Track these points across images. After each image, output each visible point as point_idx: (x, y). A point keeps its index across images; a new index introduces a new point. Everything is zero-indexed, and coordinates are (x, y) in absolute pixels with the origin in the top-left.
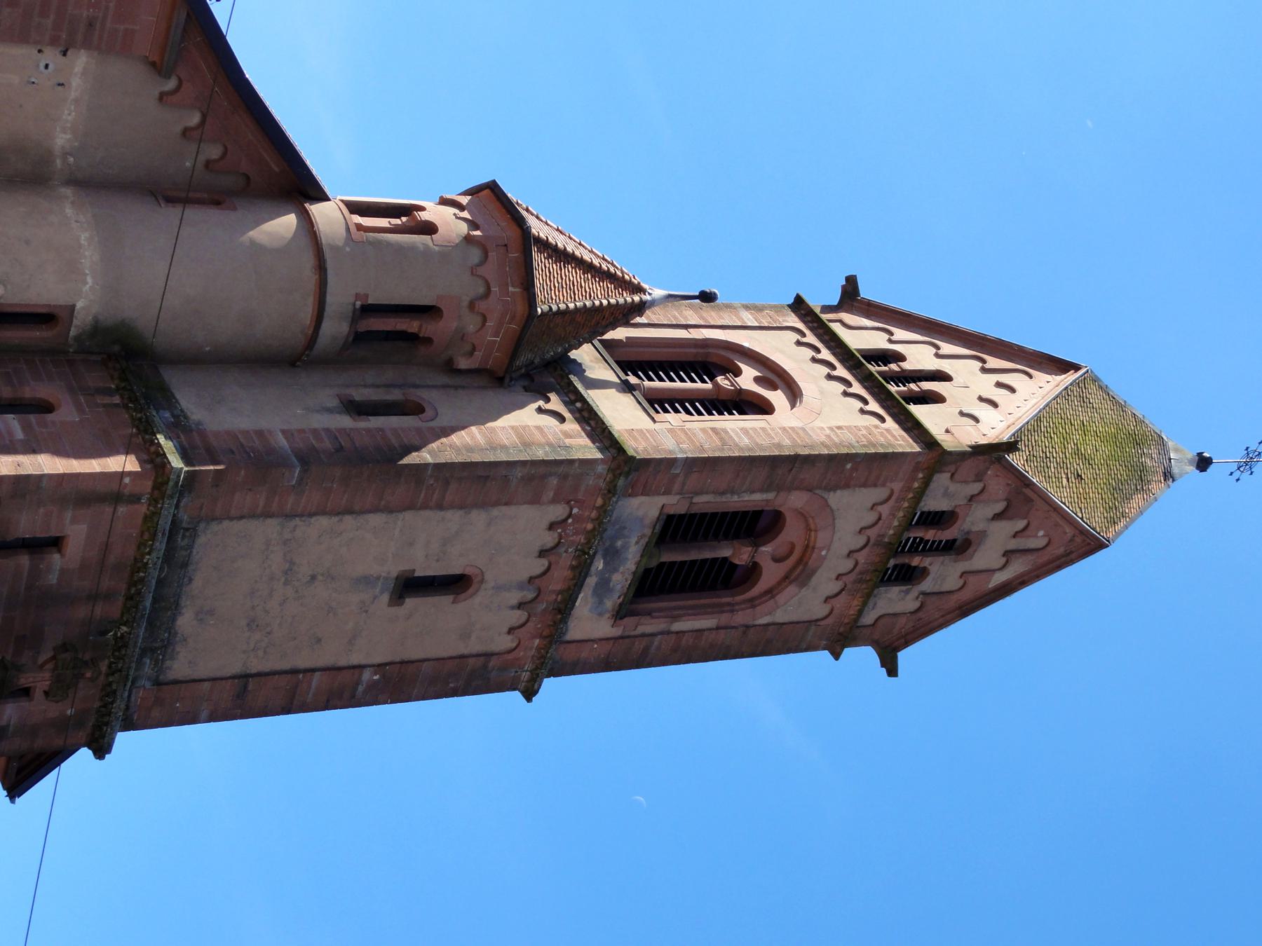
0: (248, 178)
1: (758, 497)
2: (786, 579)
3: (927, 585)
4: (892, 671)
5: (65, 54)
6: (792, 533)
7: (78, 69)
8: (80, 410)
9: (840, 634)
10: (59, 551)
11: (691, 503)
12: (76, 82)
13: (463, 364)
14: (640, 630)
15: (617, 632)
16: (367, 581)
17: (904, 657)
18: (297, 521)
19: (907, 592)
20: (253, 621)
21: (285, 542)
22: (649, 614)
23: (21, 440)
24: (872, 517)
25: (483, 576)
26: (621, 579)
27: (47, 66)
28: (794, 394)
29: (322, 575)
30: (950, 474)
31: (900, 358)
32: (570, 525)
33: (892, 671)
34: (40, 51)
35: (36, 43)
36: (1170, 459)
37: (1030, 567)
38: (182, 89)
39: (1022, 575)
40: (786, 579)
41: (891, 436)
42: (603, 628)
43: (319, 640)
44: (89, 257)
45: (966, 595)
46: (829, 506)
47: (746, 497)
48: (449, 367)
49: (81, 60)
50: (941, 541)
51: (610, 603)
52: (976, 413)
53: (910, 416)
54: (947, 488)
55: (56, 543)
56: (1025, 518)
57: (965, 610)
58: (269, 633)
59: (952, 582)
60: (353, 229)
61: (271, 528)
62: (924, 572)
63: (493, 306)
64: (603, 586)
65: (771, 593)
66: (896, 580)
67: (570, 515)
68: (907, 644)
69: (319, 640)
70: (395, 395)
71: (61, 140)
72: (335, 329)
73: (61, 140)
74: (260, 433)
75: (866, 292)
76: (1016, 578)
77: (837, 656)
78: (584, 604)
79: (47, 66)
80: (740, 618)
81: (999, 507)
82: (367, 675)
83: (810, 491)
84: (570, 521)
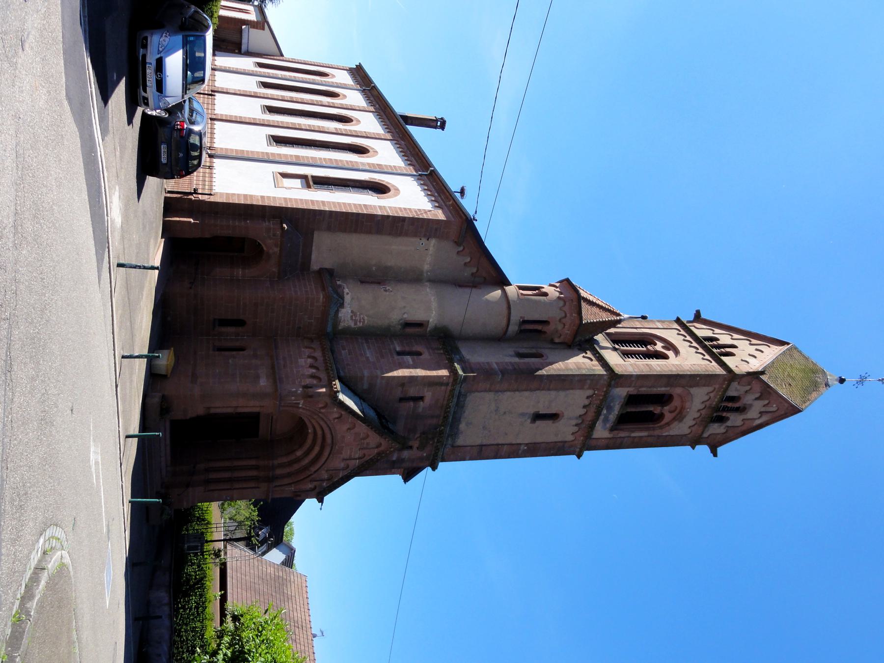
2: (674, 419)
3: (729, 423)
4: (715, 455)
5: (428, 240)
6: (676, 403)
7: (432, 245)
10: (423, 401)
12: (431, 248)
13: (557, 340)
16: (523, 415)
21: (496, 400)
28: (677, 352)
33: (715, 455)
34: (420, 239)
35: (419, 237)
39: (768, 421)
45: (744, 428)
48: (552, 342)
49: (433, 241)
51: (608, 425)
52: (747, 360)
59: (739, 422)
62: (727, 419)
63: (567, 321)
64: (606, 420)
65: (668, 424)
71: (426, 267)
72: (513, 328)
73: (426, 267)
74: (488, 363)
75: (703, 316)
76: (764, 422)
77: (693, 448)
82: (522, 447)
83: (683, 387)
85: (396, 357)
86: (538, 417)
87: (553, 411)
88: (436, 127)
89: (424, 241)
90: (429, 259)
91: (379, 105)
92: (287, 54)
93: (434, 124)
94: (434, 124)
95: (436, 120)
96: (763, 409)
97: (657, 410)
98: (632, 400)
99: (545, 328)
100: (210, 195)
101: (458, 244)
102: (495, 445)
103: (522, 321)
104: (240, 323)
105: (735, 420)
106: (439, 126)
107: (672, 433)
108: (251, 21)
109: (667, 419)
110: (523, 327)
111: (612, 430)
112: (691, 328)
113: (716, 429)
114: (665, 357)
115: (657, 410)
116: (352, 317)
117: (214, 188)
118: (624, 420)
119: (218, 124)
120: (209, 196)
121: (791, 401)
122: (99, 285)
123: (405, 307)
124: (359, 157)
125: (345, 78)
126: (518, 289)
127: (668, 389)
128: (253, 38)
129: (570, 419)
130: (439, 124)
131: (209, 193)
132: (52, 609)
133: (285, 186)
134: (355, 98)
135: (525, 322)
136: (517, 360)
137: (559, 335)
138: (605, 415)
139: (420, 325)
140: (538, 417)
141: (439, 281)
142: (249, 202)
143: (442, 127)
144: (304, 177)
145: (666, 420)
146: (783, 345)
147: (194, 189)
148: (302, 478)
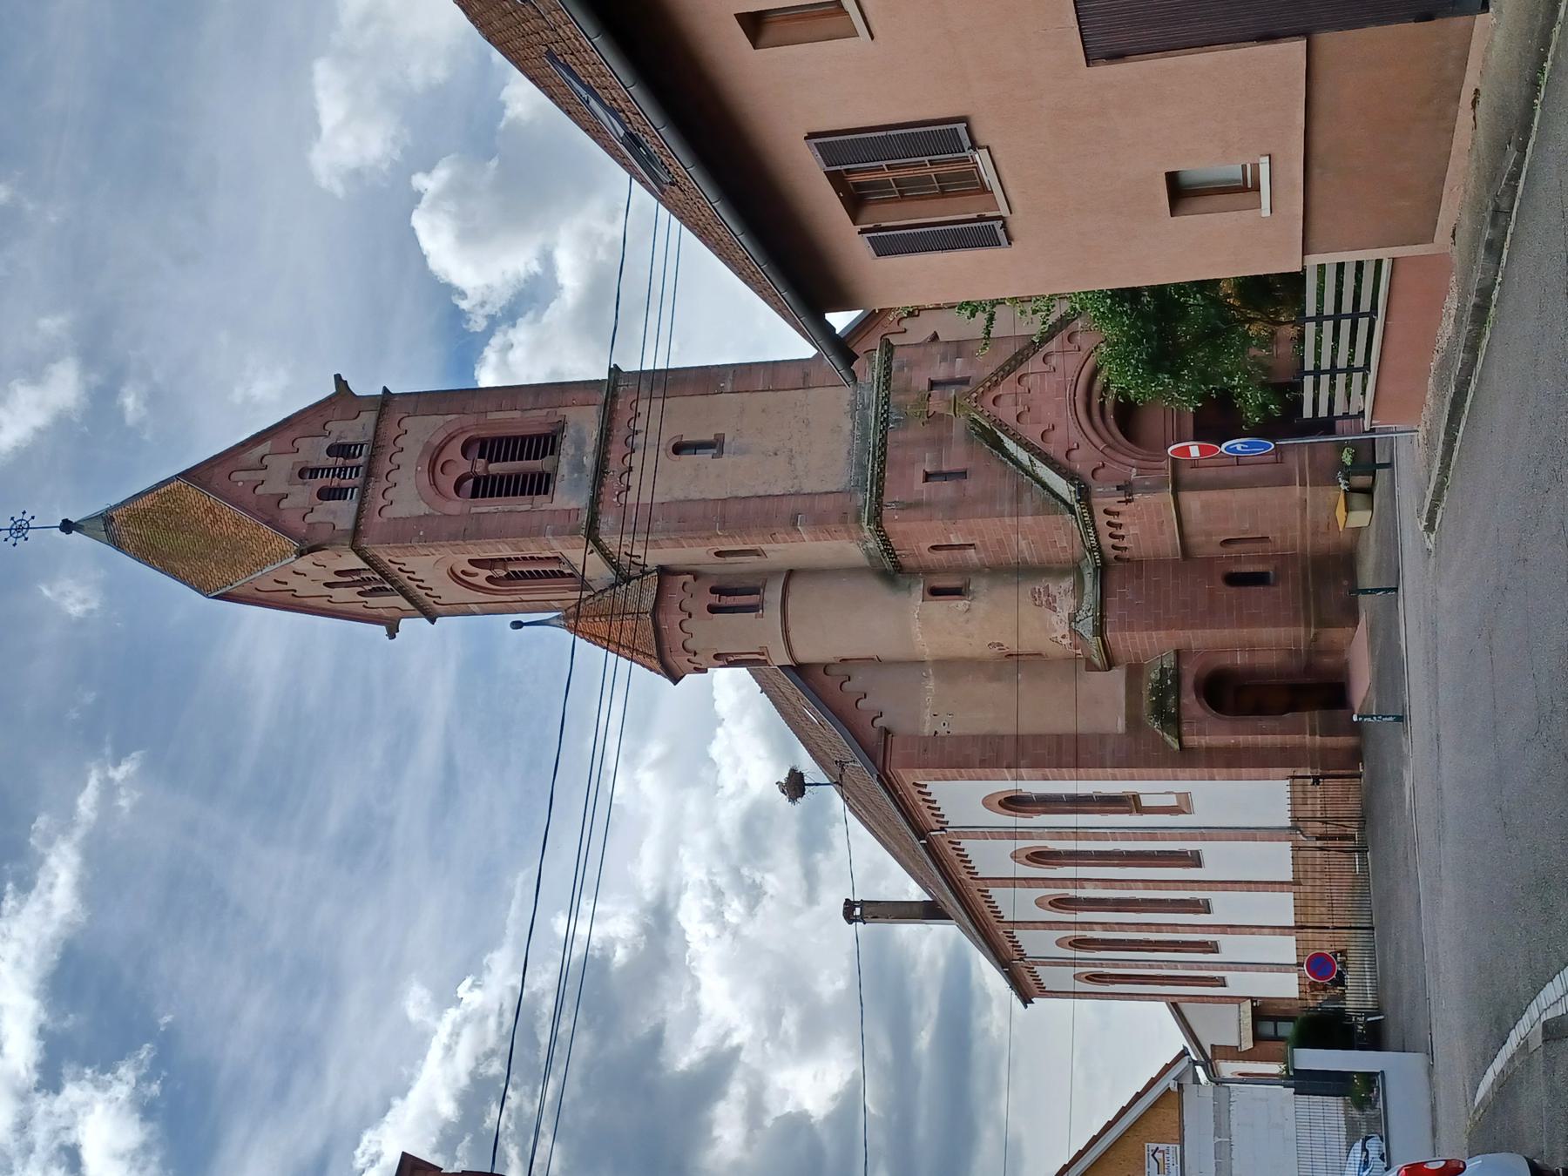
0: (826, 674)
1: (485, 510)
2: (441, 448)
3: (326, 443)
4: (338, 378)
5: (936, 733)
6: (447, 482)
7: (928, 724)
8: (918, 547)
9: (387, 406)
10: (926, 472)
11: (532, 504)
12: (928, 718)
13: (689, 578)
14: (544, 412)
15: (562, 411)
16: (742, 451)
17: (331, 389)
18: (792, 490)
19: (340, 437)
20: (807, 425)
21: (796, 477)
22: (541, 424)
23: (952, 533)
24: (389, 495)
25: (666, 453)
26: (567, 448)
27: (944, 724)
28: (453, 574)
29: (770, 456)
30: (336, 528)
31: (360, 593)
32: (616, 490)
33: (338, 378)
34: (949, 732)
35: (952, 737)
36: (105, 530)
37: (240, 457)
38: (359, 419)
39: (244, 452)
40: (441, 448)
41: (384, 555)
42: (572, 414)
43: (763, 411)
44: (916, 628)
45: (289, 435)
46: (427, 504)
47: (492, 509)
48: (696, 575)
49: (927, 730)
50: (322, 477)
51: (570, 432)
52: (315, 566)
53: (365, 560)
54: (334, 518)
55: (928, 477)
56: (259, 496)
57: (287, 423)
58: (796, 417)
59: (303, 444)
60: (766, 653)
61: (809, 486)
62: (330, 452)
63: (677, 617)
64: (579, 445)
65: (450, 438)
66: (350, 446)
67: (618, 496)
68: (329, 398)
69: (763, 411)
70: (729, 559)
71: (931, 685)
72: (773, 595)
73: (931, 685)
74: (818, 540)
75: (382, 630)
76: (251, 448)
77: (385, 390)
78: (592, 433)
79: (944, 724)
80: (469, 420)
81: (284, 504)
82: (729, 387)
83: (445, 515)
84: (617, 493)
85: (977, 542)
86: (715, 446)
87: (686, 459)
88: (862, 903)
89: (942, 731)
91: (998, 935)
92: (1162, 1008)
93: (868, 909)
96: (261, 475)
98: (540, 484)
99: (714, 599)
100: (1293, 777)
101: (887, 732)
102: (779, 390)
103: (758, 611)
104: (1234, 580)
105: (315, 452)
106: (858, 906)
107: (438, 420)
108: (1234, 1059)
109: (456, 447)
111: (561, 426)
112: (412, 608)
113: (356, 430)
114: (472, 562)
116: (1055, 601)
117: (1288, 788)
118: (546, 443)
119: (1289, 877)
120: (1295, 774)
121: (209, 496)
123: (967, 621)
124: (1046, 847)
125: (1050, 976)
126: (769, 661)
127: (474, 510)
130: (858, 911)
131: (1295, 780)
133: (1174, 795)
134: (1036, 944)
136: (764, 547)
137: (686, 588)
139: (935, 592)
140: (715, 446)
142: (1233, 770)
143: (849, 906)
144: (1142, 810)
145: (457, 445)
146: (224, 594)
147: (1318, 784)
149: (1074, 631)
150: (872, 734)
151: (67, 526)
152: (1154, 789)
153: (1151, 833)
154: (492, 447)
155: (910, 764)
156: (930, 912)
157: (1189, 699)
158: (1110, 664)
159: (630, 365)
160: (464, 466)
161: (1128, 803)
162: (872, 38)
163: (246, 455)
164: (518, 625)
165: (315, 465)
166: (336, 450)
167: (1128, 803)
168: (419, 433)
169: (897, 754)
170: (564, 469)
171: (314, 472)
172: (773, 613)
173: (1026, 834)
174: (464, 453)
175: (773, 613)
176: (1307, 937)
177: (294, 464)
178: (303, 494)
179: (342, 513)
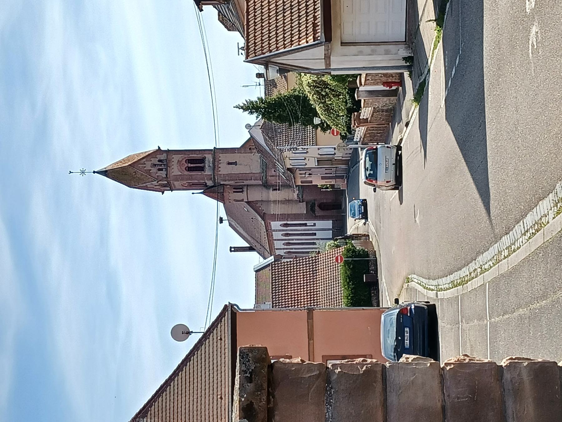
14: (201, 155)
16: (240, 165)
33: (158, 146)
45: (149, 158)
51: (207, 159)
71: (272, 205)
72: (245, 189)
73: (272, 205)
86: (235, 163)
88: (234, 248)
90: (272, 208)
93: (236, 249)
94: (236, 249)
95: (234, 251)
96: (145, 165)
97: (190, 165)
110: (241, 190)
113: (163, 157)
115: (190, 165)
122: (491, 221)
128: (313, 202)
129: (223, 163)
132: (496, 147)
135: (242, 192)
138: (210, 164)
140: (235, 163)
141: (268, 202)
145: (184, 160)
148: (235, 397)
149: (298, 197)
150: (262, 214)
151: (94, 172)
152: (309, 223)
153: (308, 230)
154: (191, 161)
155: (269, 219)
156: (251, 249)
157: (317, 208)
158: (303, 202)
159: (217, 147)
160: (186, 165)
161: (305, 225)
162: (238, 43)
163: (141, 161)
164: (193, 193)
165: (155, 164)
166: (160, 161)
167: (305, 225)
168: (176, 158)
169: (267, 217)
170: (207, 166)
171: (155, 165)
172: (245, 193)
173: (286, 230)
174: (186, 162)
175: (245, 193)
176: (195, 399)
177: (152, 163)
178: (154, 170)
179: (163, 174)
